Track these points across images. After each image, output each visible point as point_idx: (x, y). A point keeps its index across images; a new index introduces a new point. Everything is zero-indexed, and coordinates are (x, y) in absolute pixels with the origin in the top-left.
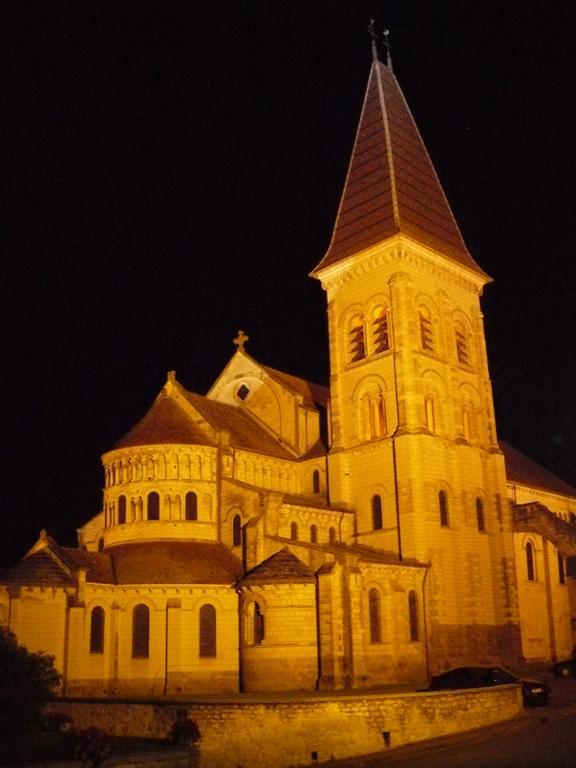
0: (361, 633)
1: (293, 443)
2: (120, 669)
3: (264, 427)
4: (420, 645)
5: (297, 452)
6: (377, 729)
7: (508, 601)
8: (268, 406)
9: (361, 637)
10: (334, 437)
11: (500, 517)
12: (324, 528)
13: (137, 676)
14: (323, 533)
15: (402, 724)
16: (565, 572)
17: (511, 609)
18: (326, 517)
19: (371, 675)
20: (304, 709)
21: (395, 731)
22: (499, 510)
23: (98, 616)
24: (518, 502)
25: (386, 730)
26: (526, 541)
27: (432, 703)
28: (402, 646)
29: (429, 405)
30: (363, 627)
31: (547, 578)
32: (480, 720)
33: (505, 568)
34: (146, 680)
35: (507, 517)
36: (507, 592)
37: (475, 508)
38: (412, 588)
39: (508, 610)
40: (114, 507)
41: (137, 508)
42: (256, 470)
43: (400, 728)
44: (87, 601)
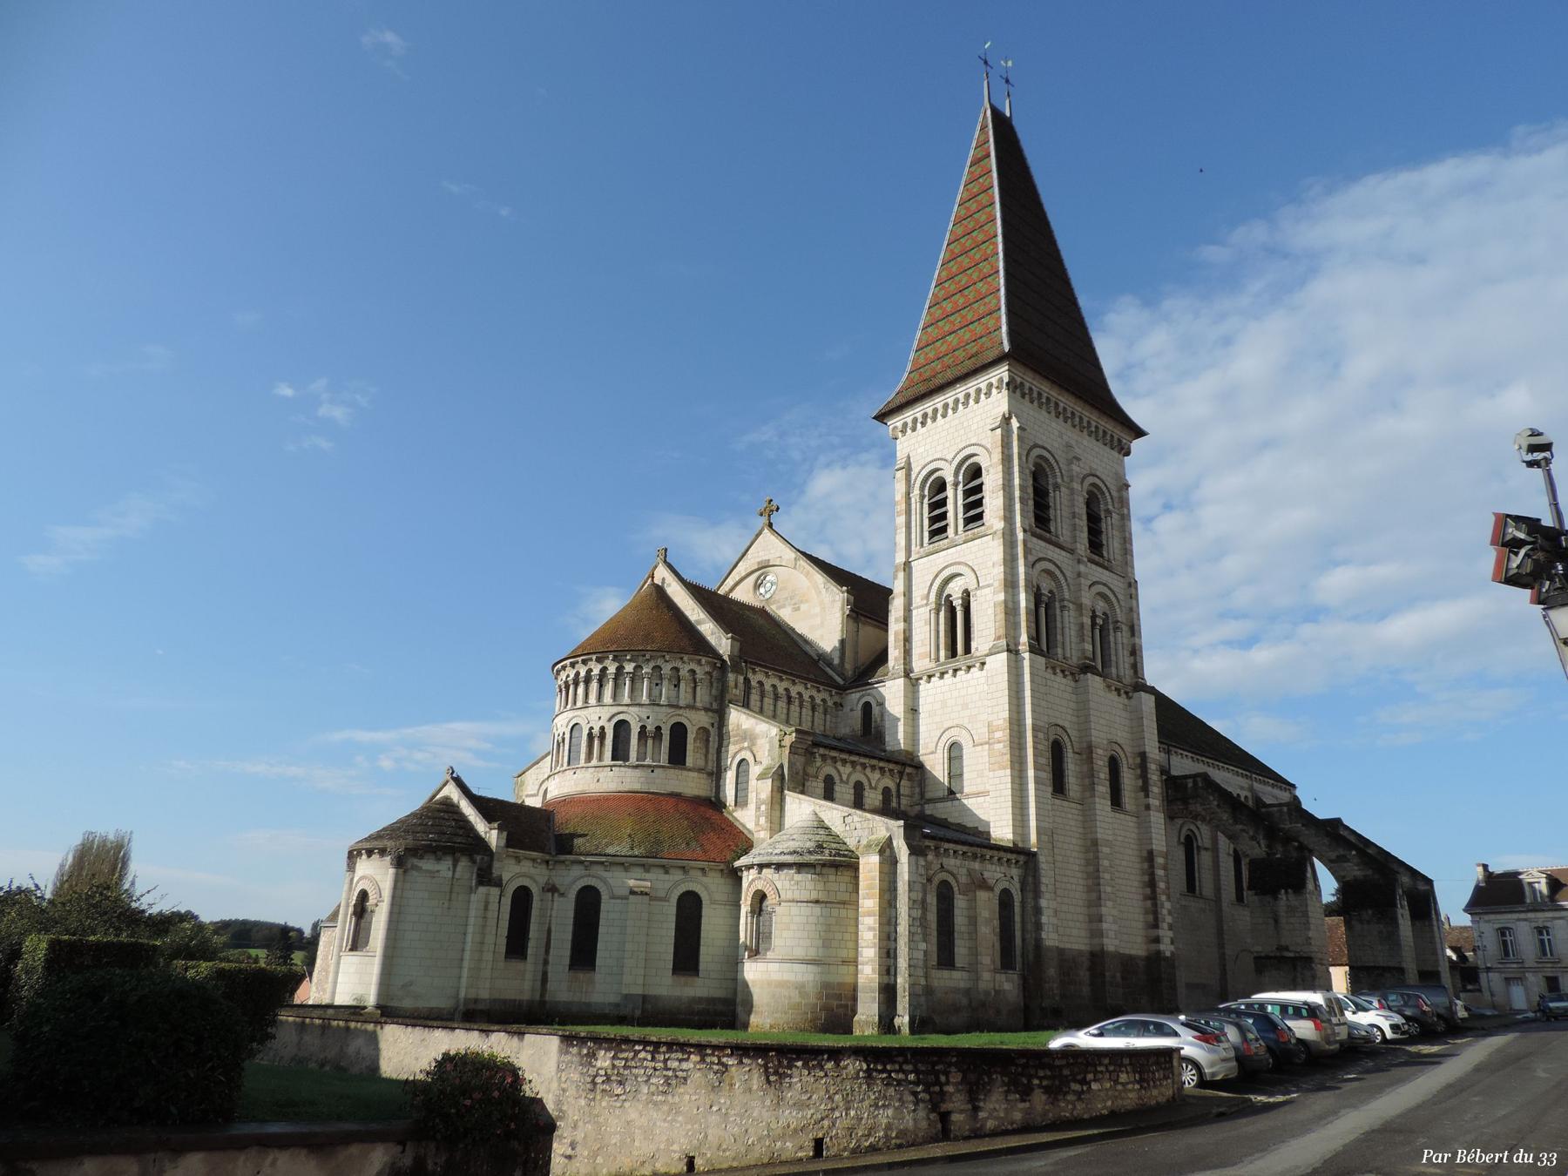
1: (836, 661)
4: (1015, 976)
5: (841, 675)
7: (1156, 919)
8: (803, 607)
11: (1145, 789)
16: (1245, 885)
23: (522, 898)
24: (1174, 773)
26: (1184, 832)
27: (1025, 1066)
28: (986, 976)
29: (1042, 611)
30: (925, 940)
33: (1152, 866)
35: (1156, 790)
38: (1005, 885)
39: (1153, 933)
41: (596, 742)
44: (506, 877)
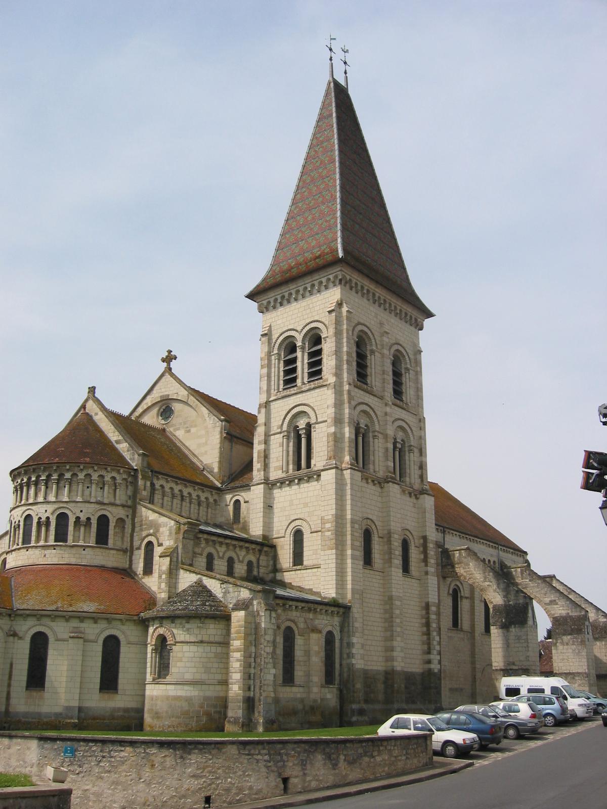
0: (271, 673)
2: (13, 701)
3: (186, 452)
6: (276, 774)
8: (193, 430)
9: (272, 678)
10: (391, 464)
12: (242, 562)
13: (32, 709)
14: (240, 567)
15: (303, 769)
17: (432, 657)
18: (224, 546)
19: (281, 719)
20: (201, 750)
21: (296, 777)
22: (425, 552)
25: (286, 775)
29: (360, 439)
31: (473, 626)
32: (386, 769)
33: (428, 613)
34: (39, 714)
36: (429, 639)
37: (400, 549)
38: (329, 628)
40: (19, 526)
41: (43, 529)
42: (173, 496)
43: (301, 773)
